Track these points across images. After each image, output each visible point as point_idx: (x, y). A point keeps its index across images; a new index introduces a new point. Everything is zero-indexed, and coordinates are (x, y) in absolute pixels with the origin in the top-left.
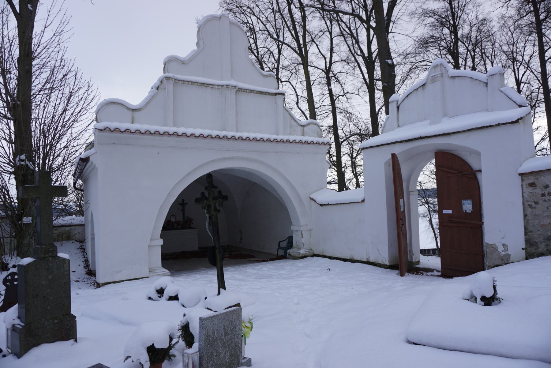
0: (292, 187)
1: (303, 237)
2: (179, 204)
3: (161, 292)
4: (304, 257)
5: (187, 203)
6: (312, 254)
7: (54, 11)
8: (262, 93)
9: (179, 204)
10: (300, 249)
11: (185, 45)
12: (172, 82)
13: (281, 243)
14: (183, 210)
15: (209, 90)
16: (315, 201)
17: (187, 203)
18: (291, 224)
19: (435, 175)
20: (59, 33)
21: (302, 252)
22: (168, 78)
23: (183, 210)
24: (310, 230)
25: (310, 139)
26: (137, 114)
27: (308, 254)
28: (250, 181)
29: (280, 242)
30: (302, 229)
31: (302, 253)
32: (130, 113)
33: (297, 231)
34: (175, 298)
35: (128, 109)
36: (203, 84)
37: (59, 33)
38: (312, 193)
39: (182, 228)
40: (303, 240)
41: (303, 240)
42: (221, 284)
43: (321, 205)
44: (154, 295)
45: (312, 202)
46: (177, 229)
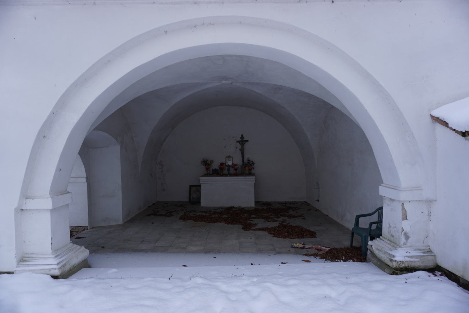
0: (367, 77)
1: (405, 218)
2: (237, 142)
4: (409, 269)
5: (247, 141)
6: (430, 264)
9: (237, 142)
10: (395, 245)
13: (361, 219)
14: (242, 151)
16: (445, 124)
17: (247, 141)
18: (380, 181)
21: (401, 256)
23: (242, 151)
24: (429, 202)
27: (417, 263)
28: (325, 103)
29: (358, 217)
30: (403, 196)
31: (398, 258)
33: (392, 200)
38: (439, 105)
39: (236, 175)
40: (406, 225)
41: (406, 225)
43: (464, 134)
45: (439, 128)
46: (231, 175)
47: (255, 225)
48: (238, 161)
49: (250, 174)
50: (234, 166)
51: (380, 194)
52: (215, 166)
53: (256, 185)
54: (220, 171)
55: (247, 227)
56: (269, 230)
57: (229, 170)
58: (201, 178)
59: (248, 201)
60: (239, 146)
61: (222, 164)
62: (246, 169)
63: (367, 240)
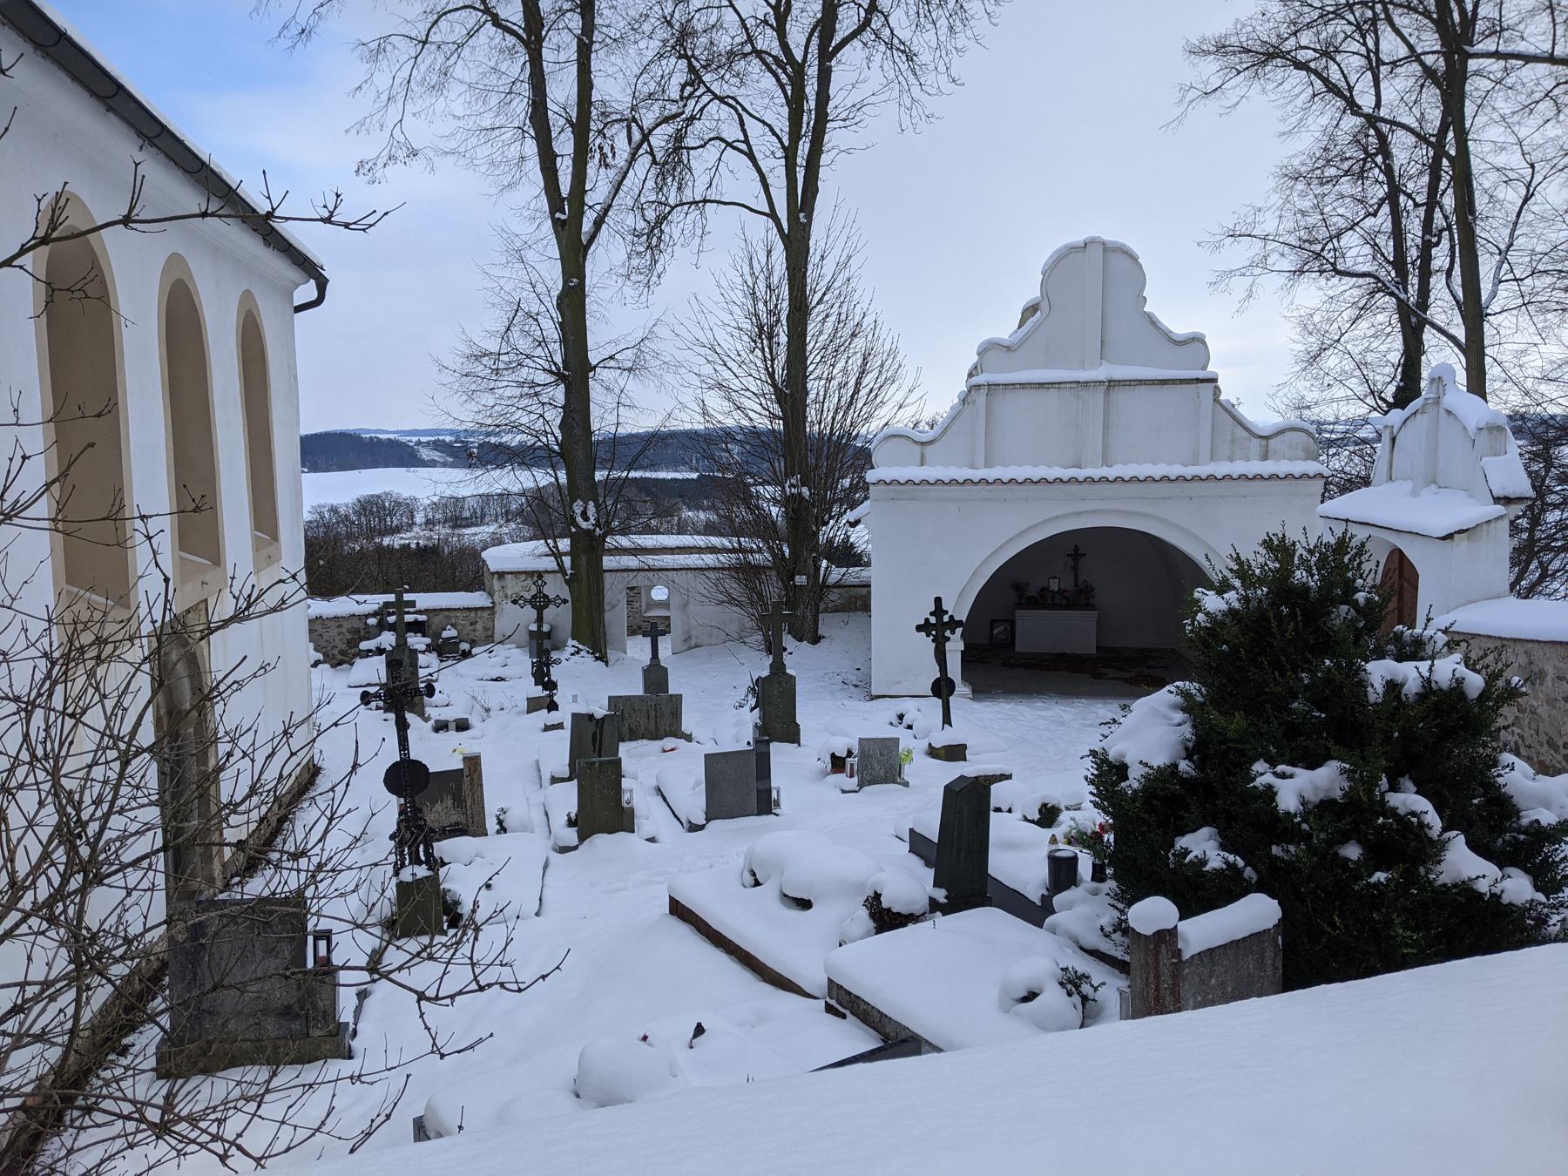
3: (901, 717)
7: (838, 226)
8: (1164, 382)
11: (1005, 327)
12: (984, 391)
14: (1075, 569)
15: (1053, 392)
19: (160, 803)
20: (843, 265)
22: (978, 387)
23: (1075, 569)
25: (1282, 467)
26: (929, 449)
32: (918, 448)
34: (910, 727)
35: (915, 442)
36: (1041, 385)
37: (843, 265)
39: (1067, 607)
42: (947, 720)
44: (896, 721)
47: (413, 604)
48: (1068, 584)
49: (1088, 606)
50: (1062, 592)
51: (990, 872)
52: (1032, 591)
53: (1098, 622)
54: (1043, 600)
55: (1098, 676)
56: (1126, 680)
57: (1053, 598)
58: (1019, 614)
59: (1086, 644)
60: (1070, 562)
61: (1044, 589)
62: (1080, 598)
63: (1343, 761)
